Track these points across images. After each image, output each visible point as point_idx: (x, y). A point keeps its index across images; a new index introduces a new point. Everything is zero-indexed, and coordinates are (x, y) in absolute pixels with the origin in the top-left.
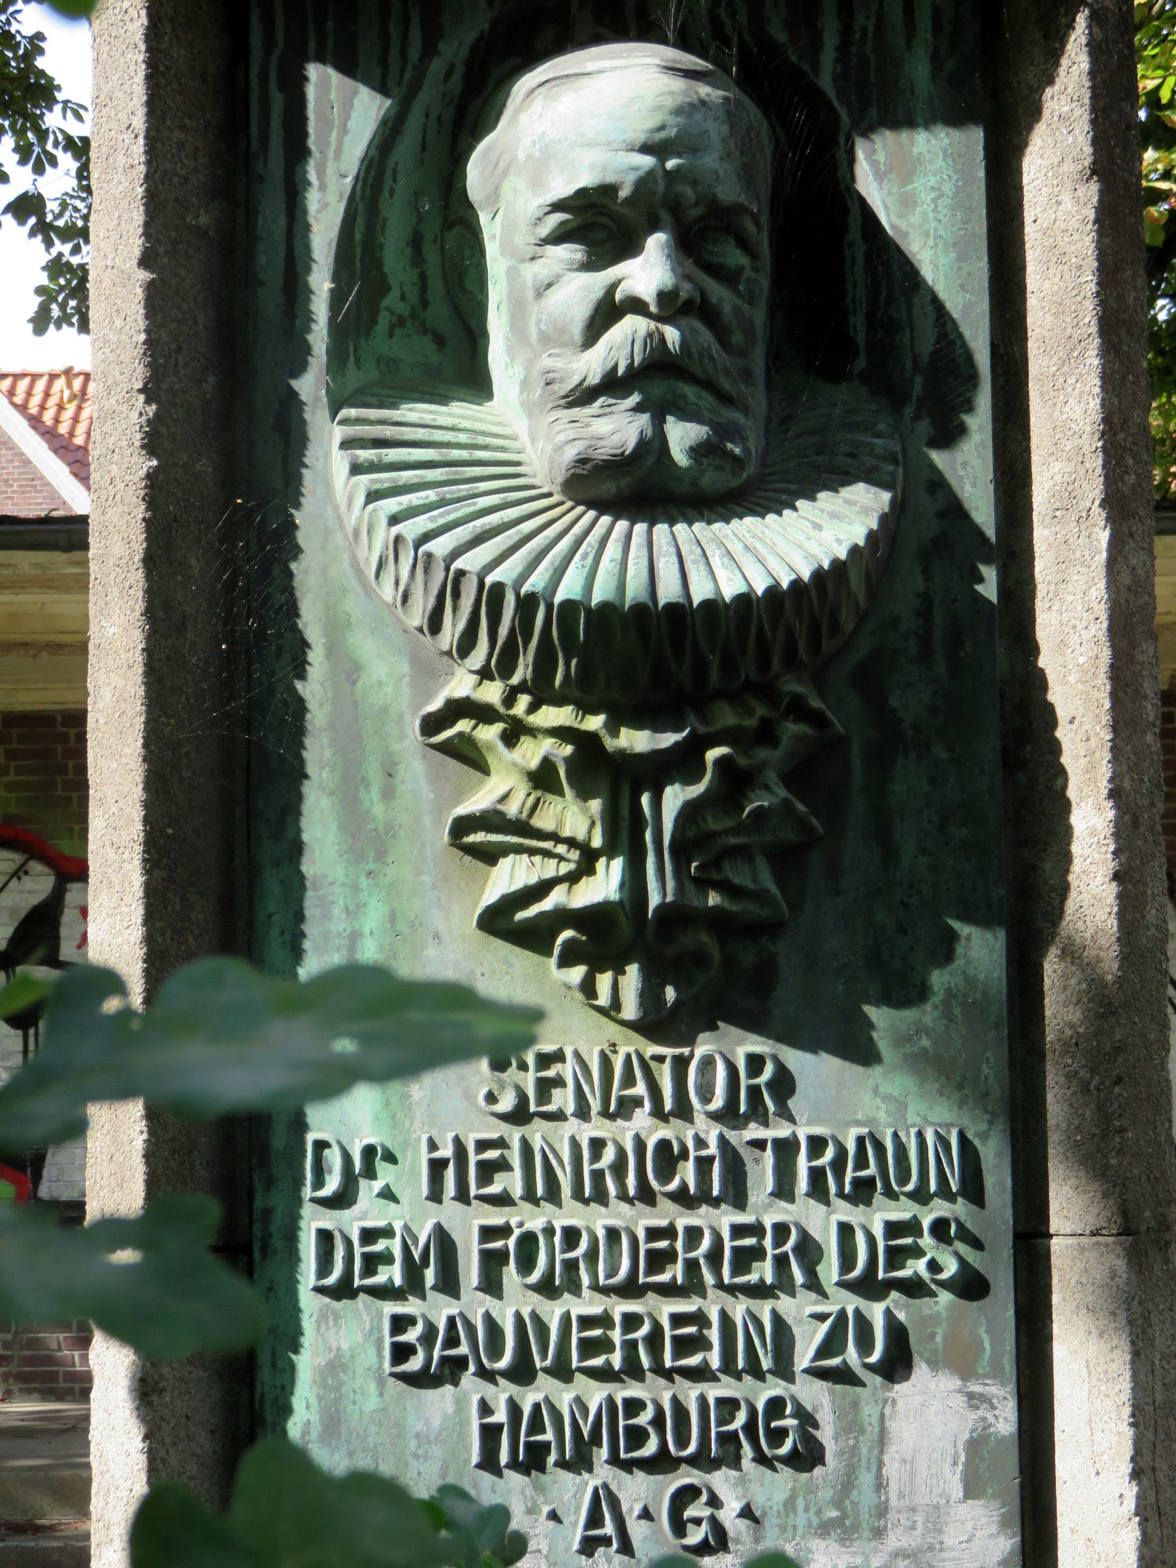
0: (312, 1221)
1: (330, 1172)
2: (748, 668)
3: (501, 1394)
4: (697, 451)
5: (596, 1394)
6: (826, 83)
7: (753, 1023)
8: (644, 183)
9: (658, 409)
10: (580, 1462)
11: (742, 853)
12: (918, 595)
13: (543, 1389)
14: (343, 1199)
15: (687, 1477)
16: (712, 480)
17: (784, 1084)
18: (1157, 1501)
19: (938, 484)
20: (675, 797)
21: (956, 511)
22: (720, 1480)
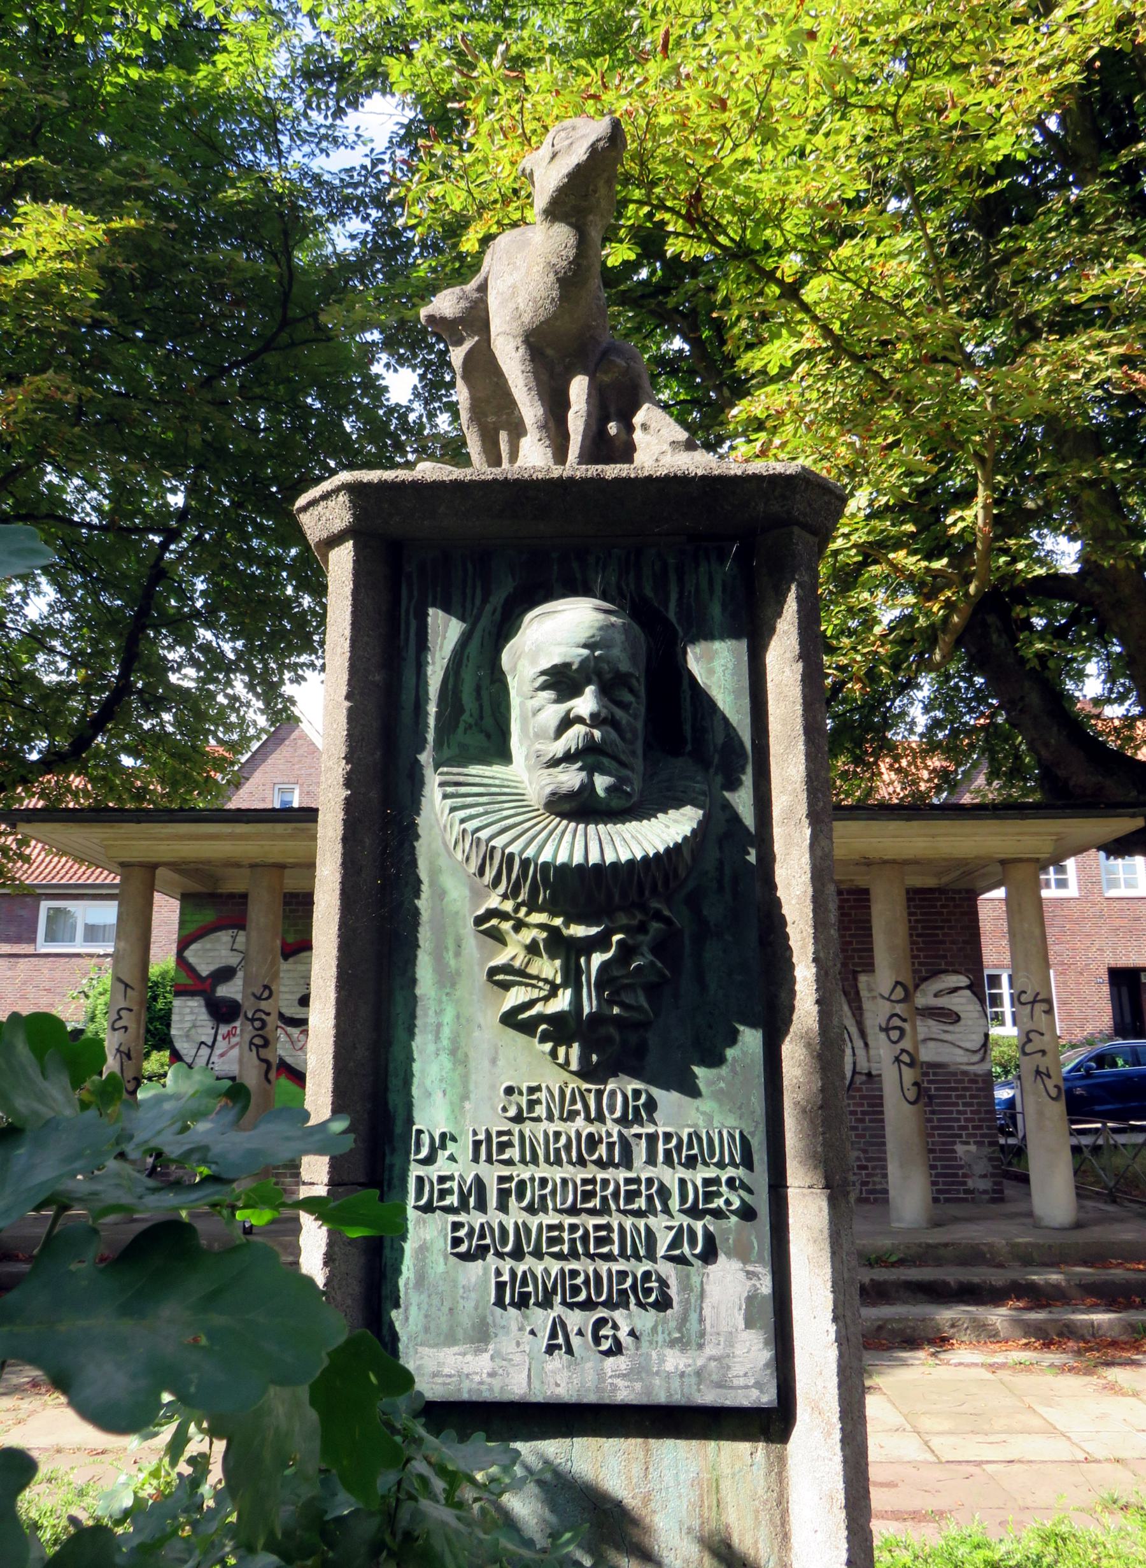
0: (415, 1171)
5: (555, 1267)
7: (635, 1074)
8: (584, 662)
9: (590, 770)
11: (630, 987)
14: (429, 1160)
15: (602, 1313)
19: (727, 806)
21: (736, 818)
22: (619, 1315)
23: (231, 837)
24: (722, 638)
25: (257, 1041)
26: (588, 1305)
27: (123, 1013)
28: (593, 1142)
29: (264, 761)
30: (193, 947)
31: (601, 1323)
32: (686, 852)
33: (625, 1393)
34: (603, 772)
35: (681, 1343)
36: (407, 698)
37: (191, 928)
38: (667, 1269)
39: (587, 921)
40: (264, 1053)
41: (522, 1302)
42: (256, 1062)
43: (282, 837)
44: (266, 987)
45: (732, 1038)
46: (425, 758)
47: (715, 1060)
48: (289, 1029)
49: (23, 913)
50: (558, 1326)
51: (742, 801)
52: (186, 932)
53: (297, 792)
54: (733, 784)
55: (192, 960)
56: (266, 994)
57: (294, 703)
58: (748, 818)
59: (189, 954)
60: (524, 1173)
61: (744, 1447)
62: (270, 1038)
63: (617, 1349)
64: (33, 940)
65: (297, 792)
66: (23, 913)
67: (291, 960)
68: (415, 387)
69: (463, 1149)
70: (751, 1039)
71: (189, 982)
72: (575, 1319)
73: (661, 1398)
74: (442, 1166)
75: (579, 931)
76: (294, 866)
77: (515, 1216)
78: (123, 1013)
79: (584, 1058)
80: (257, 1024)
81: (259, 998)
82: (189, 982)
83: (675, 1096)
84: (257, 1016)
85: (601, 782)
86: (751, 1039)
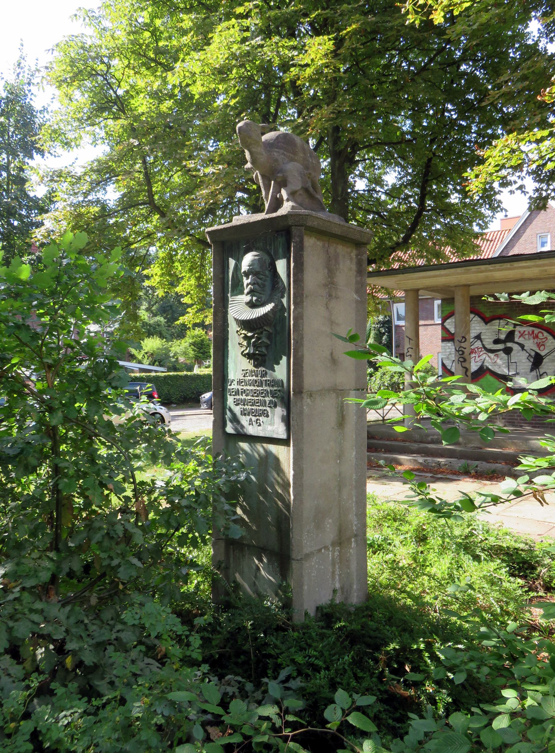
0: (229, 387)
1: (438, 306)
2: (259, 326)
3: (243, 407)
4: (256, 300)
5: (250, 407)
6: (272, 253)
7: (264, 366)
8: (248, 270)
9: (252, 296)
10: (249, 415)
11: (261, 347)
12: (337, 298)
13: (246, 407)
14: (230, 385)
15: (258, 417)
16: (258, 303)
17: (266, 373)
18: (483, 345)
19: (282, 302)
20: (253, 340)
21: (283, 305)
22: (260, 418)
23: (430, 277)
24: (282, 259)
25: (461, 360)
26: (255, 416)
27: (409, 350)
28: (256, 381)
29: (531, 223)
30: (448, 321)
31: (257, 420)
32: (271, 315)
33: (261, 434)
34: (255, 296)
35: (270, 424)
36: (226, 281)
37: (446, 313)
38: (268, 409)
39: (251, 332)
40: (464, 364)
41: (245, 415)
42: (461, 368)
43: (460, 274)
44: (463, 337)
45: (281, 358)
46: (229, 295)
47: (278, 363)
48: (490, 354)
49: (428, 306)
50: (251, 420)
51: (284, 301)
52: (444, 315)
53: (549, 237)
54: (283, 297)
55: (448, 327)
56: (464, 340)
57: (502, 203)
58: (285, 305)
59: (445, 324)
60: (245, 388)
61: (283, 447)
62: (467, 358)
63: (260, 425)
64: (433, 318)
65: (549, 237)
66: (428, 306)
67: (489, 324)
68: (539, 30)
69: (235, 382)
70: (284, 358)
71: (447, 336)
72: (254, 419)
73: (267, 435)
74: (232, 387)
75: (250, 334)
76: (474, 285)
77: (244, 397)
78: (409, 350)
79: (254, 363)
80: (461, 353)
81: (461, 342)
82: (447, 336)
83: (271, 371)
84: (461, 349)
85: (254, 298)
86: (284, 358)
